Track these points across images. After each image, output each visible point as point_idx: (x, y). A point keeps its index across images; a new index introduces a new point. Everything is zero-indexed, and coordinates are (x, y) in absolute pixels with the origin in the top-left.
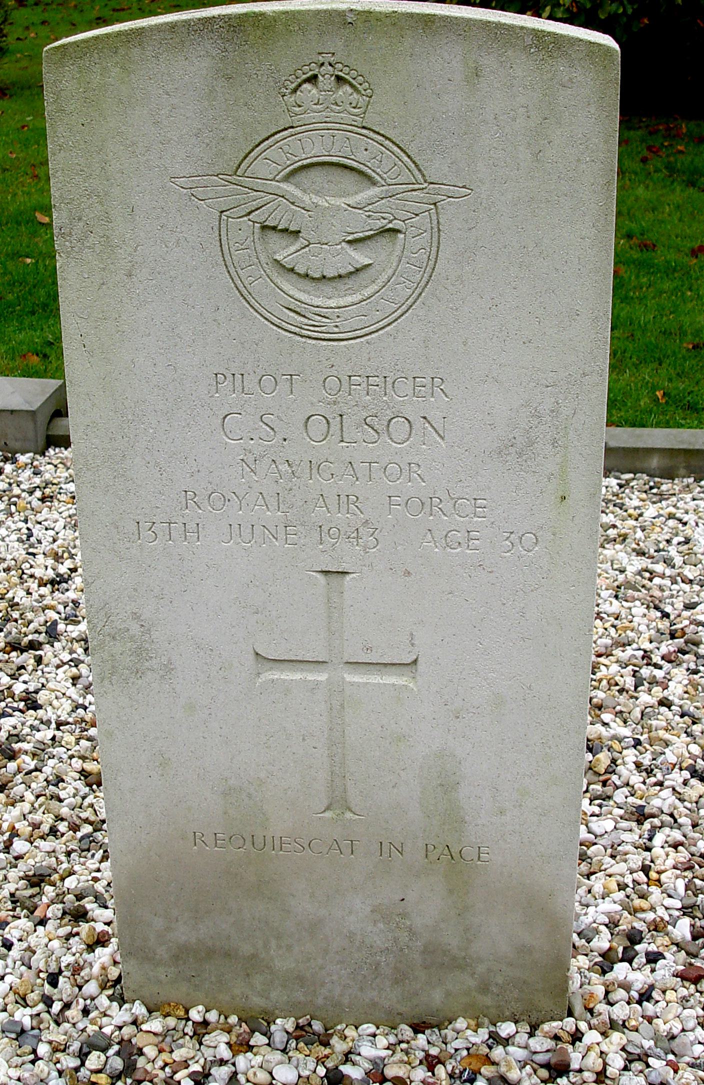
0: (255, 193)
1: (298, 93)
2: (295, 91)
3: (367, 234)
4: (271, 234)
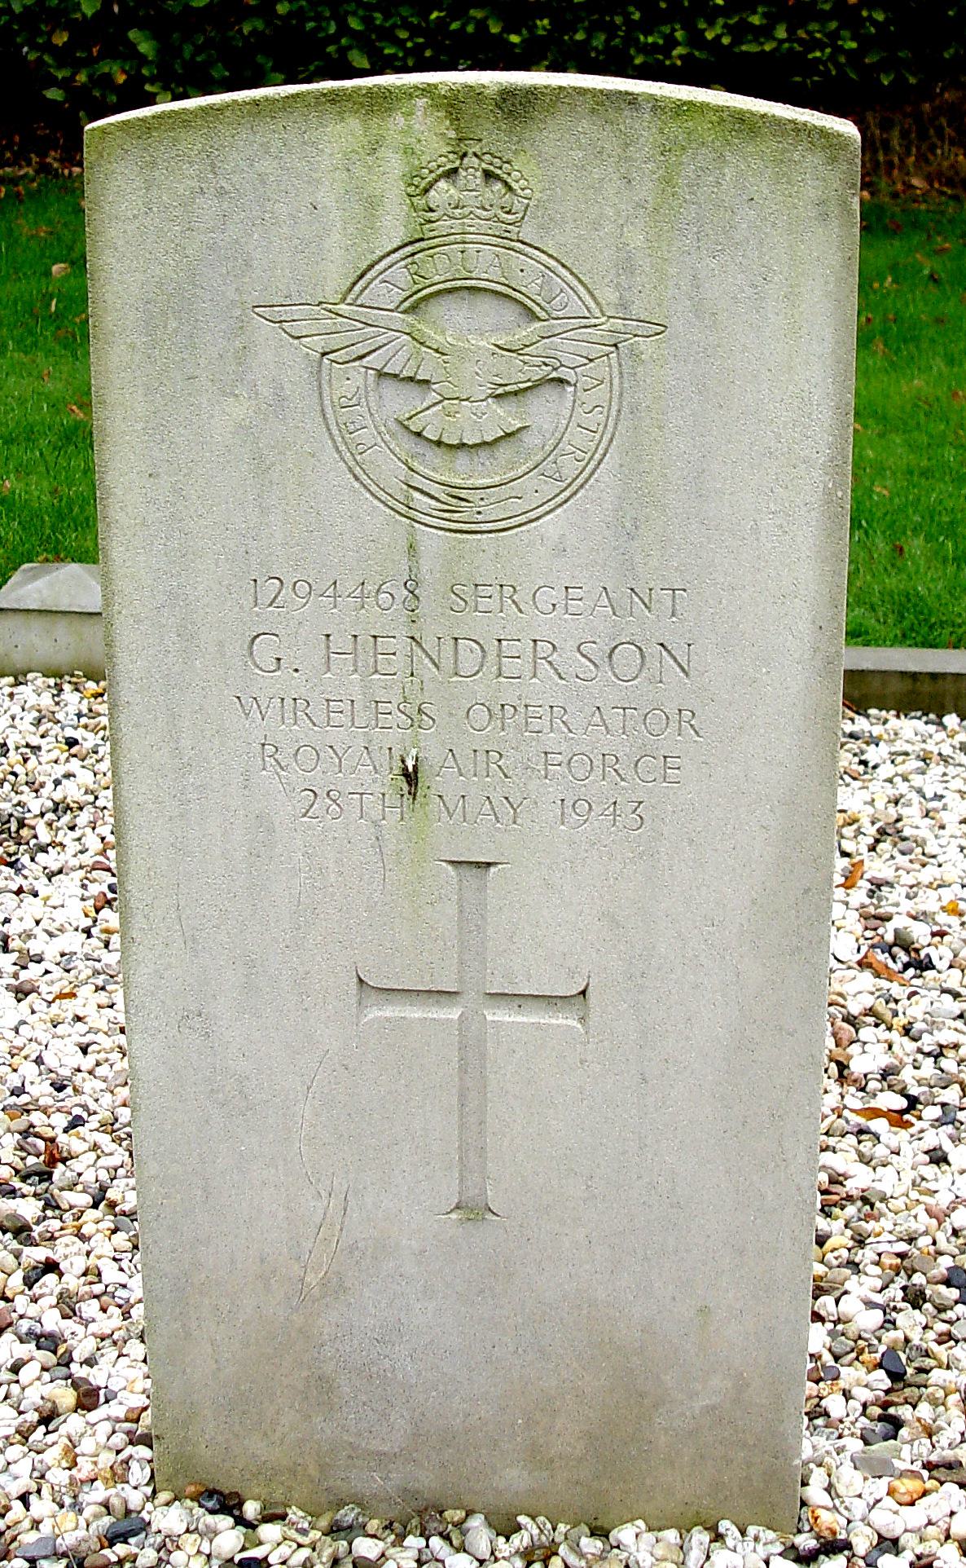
1: (432, 193)
2: (426, 191)
3: (522, 386)
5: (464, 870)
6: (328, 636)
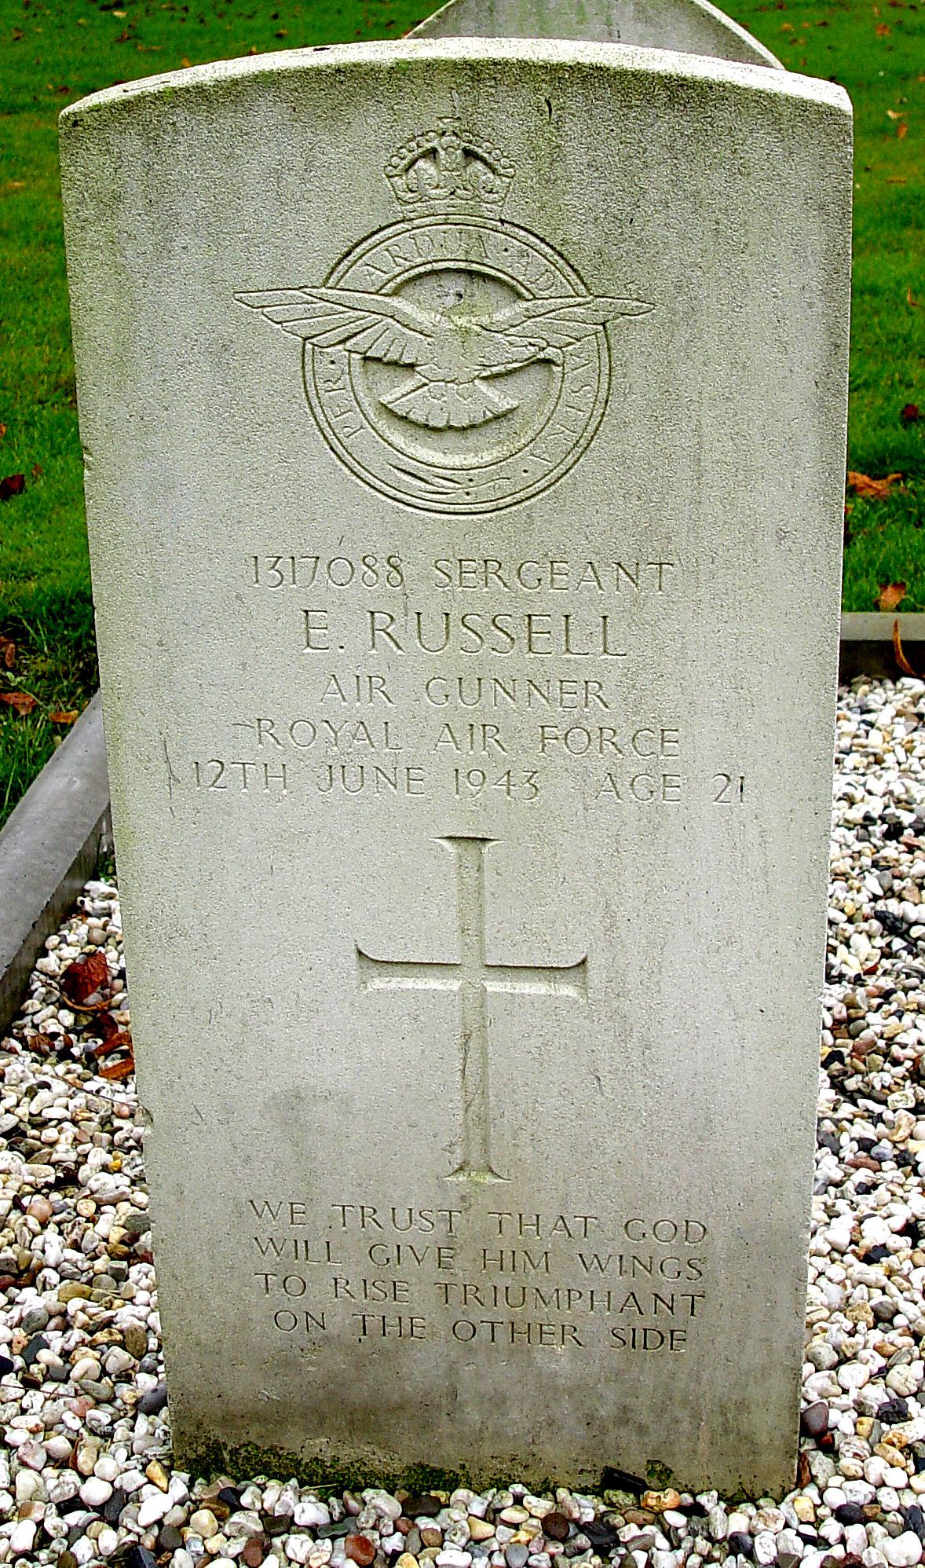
0: (351, 313)
3: (510, 366)
4: (374, 366)
5: (464, 844)
6: (605, 618)
